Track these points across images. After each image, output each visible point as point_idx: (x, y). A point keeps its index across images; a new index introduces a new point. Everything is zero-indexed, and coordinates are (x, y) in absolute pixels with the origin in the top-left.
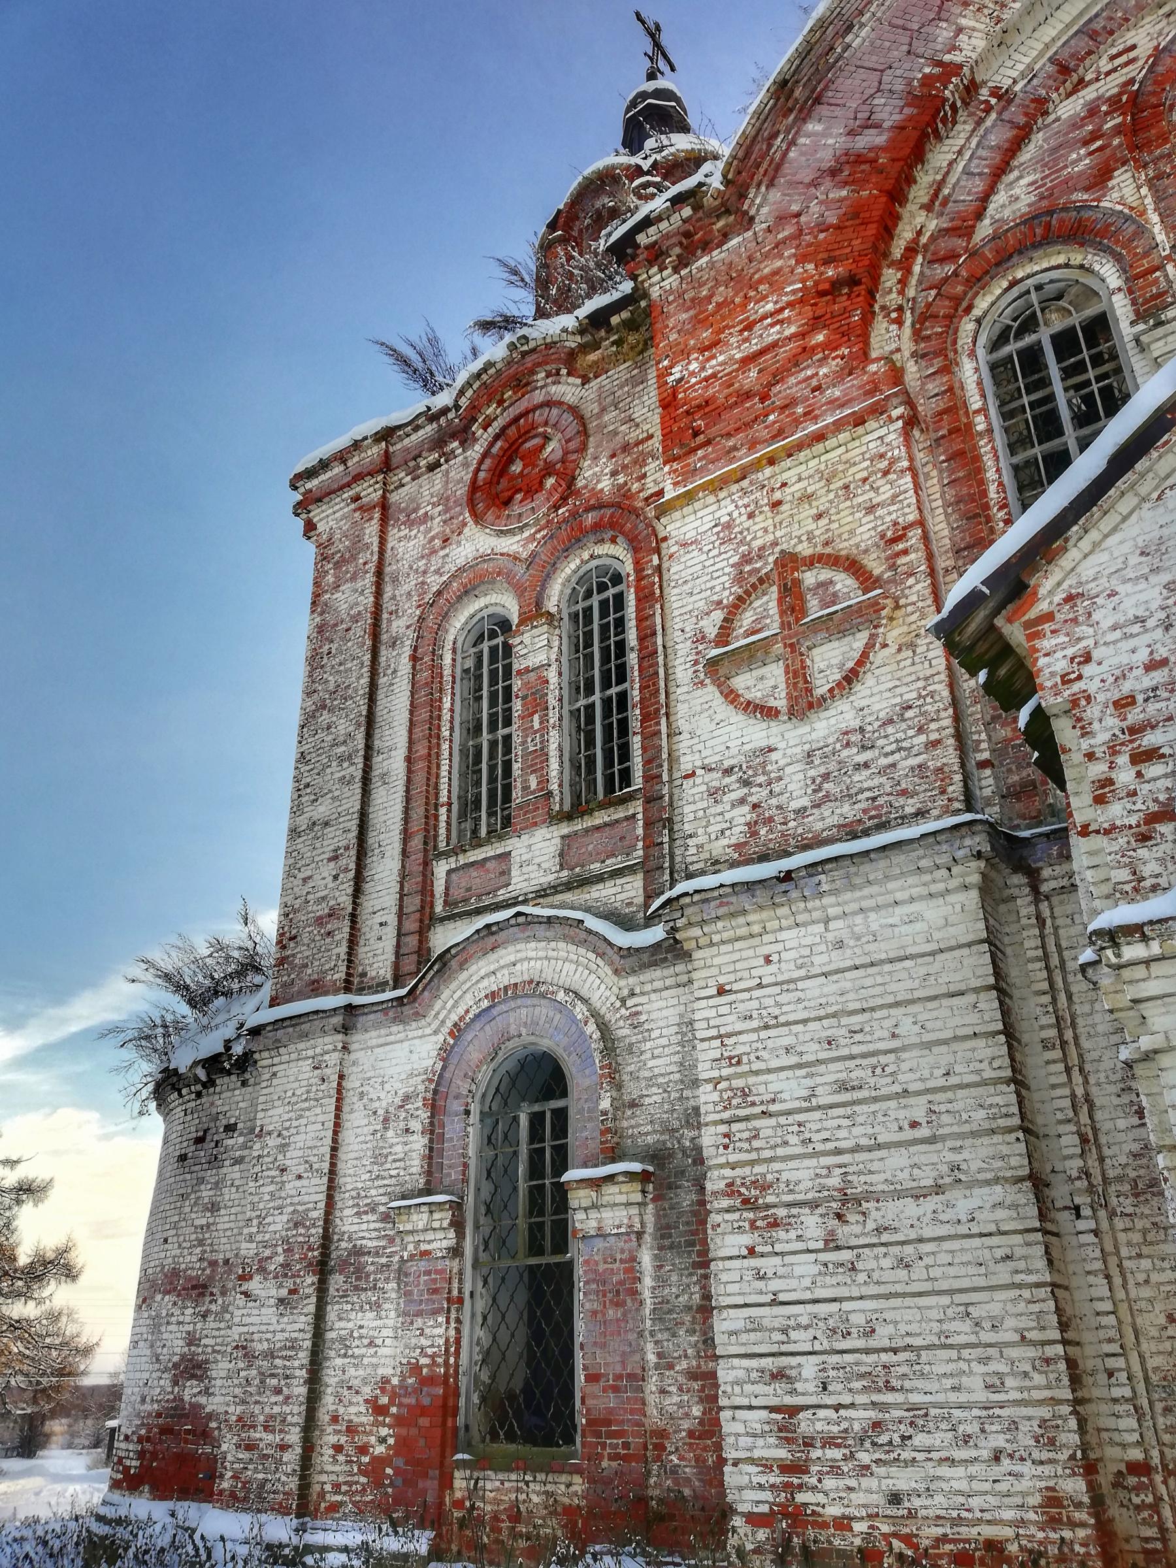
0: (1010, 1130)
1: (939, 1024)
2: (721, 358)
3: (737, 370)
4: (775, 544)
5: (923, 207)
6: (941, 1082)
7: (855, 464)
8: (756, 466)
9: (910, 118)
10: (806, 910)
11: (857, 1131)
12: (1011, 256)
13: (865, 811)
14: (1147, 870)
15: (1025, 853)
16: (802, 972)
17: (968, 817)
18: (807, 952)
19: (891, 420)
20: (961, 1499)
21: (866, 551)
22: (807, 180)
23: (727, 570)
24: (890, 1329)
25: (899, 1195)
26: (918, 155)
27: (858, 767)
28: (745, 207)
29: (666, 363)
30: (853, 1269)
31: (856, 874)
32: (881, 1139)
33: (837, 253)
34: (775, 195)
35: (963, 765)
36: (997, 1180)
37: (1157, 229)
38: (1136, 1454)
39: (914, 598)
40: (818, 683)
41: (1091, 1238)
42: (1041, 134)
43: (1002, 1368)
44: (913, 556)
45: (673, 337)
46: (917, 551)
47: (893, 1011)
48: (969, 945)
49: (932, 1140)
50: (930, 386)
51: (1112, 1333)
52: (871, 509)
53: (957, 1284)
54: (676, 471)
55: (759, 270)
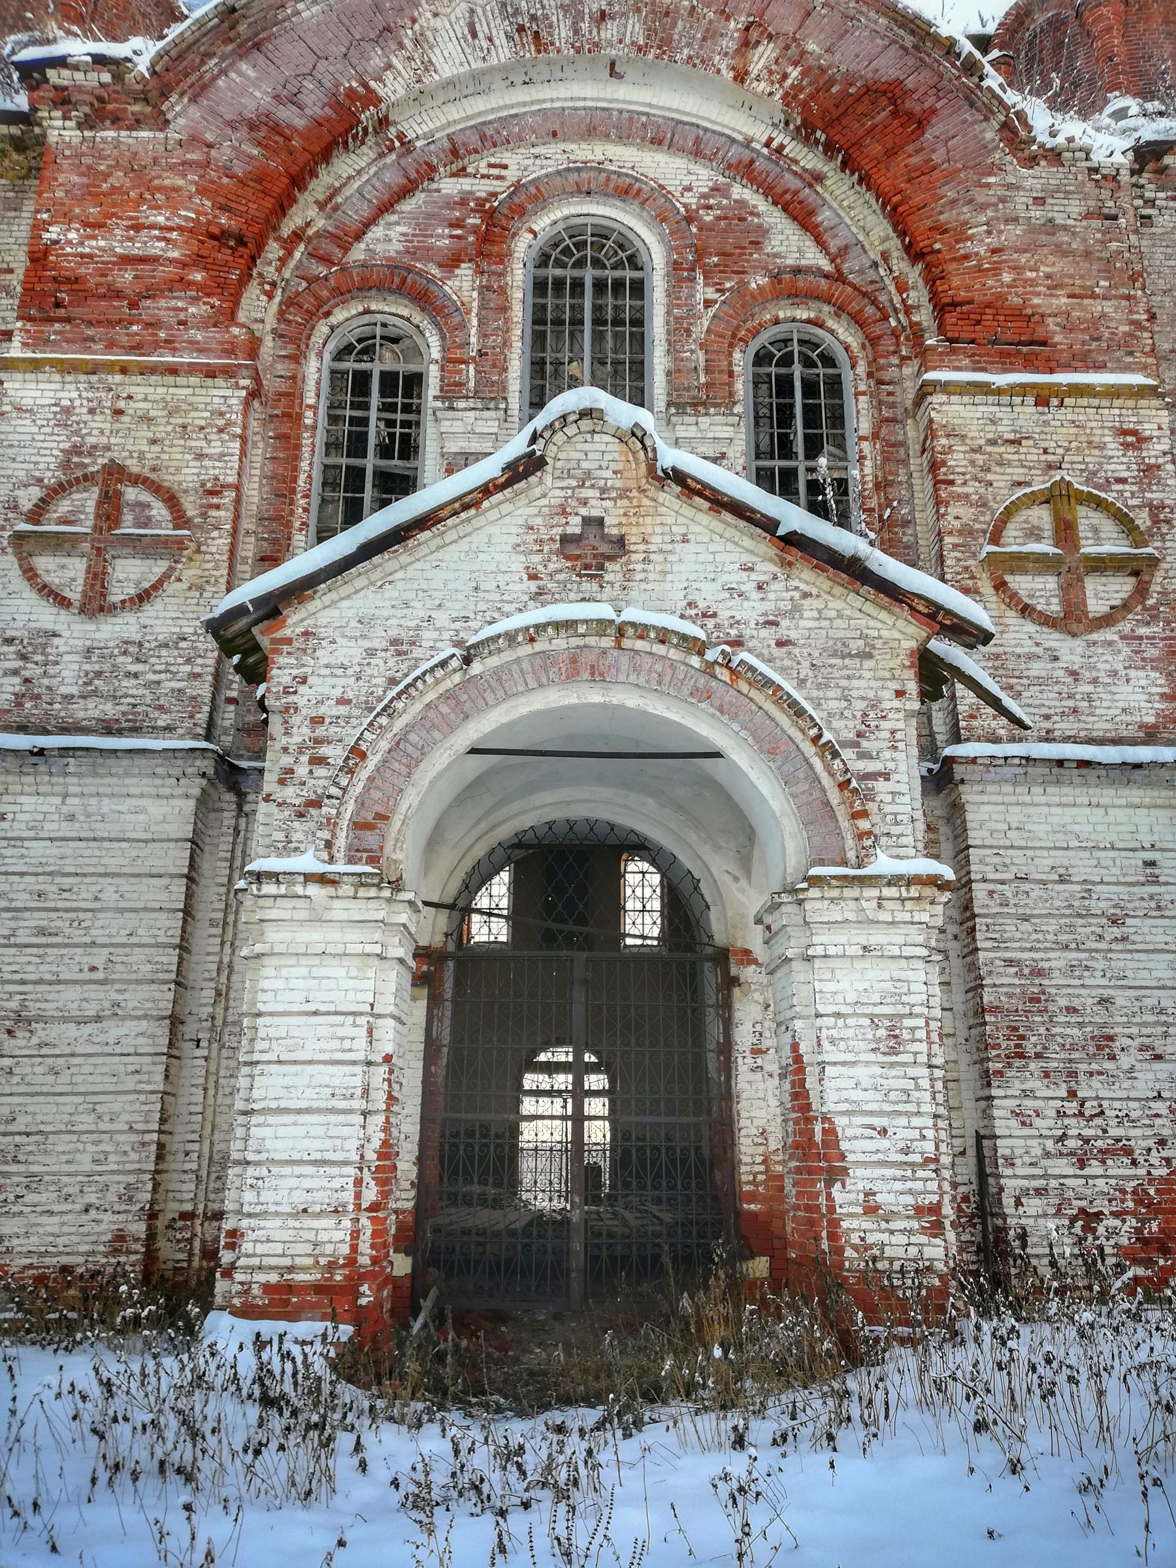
0: (166, 982)
1: (135, 896)
2: (102, 243)
3: (114, 264)
4: (107, 448)
5: (317, 202)
6: (124, 940)
7: (197, 410)
8: (109, 367)
9: (328, 120)
10: (50, 783)
11: (43, 968)
12: (371, 288)
13: (124, 713)
14: (296, 837)
15: (240, 779)
16: (32, 834)
17: (203, 744)
18: (41, 817)
19: (237, 386)
20: (51, 1239)
21: (186, 491)
22: (228, 117)
23: (56, 452)
24: (29, 1118)
25: (65, 1020)
26: (326, 155)
27: (128, 675)
28: (164, 108)
29: (45, 216)
30: (11, 1073)
31: (102, 765)
32: (62, 977)
33: (234, 205)
34: (195, 112)
35: (213, 699)
36: (145, 1017)
37: (473, 331)
38: (188, 1207)
39: (214, 549)
40: (114, 590)
41: (202, 1062)
42: (423, 195)
43: (108, 1148)
44: (222, 513)
45: (60, 194)
46: (227, 510)
47: (101, 880)
48: (177, 840)
49: (102, 982)
50: (279, 366)
51: (197, 1127)
52: (200, 457)
53: (91, 1089)
54: (28, 331)
55: (159, 177)
